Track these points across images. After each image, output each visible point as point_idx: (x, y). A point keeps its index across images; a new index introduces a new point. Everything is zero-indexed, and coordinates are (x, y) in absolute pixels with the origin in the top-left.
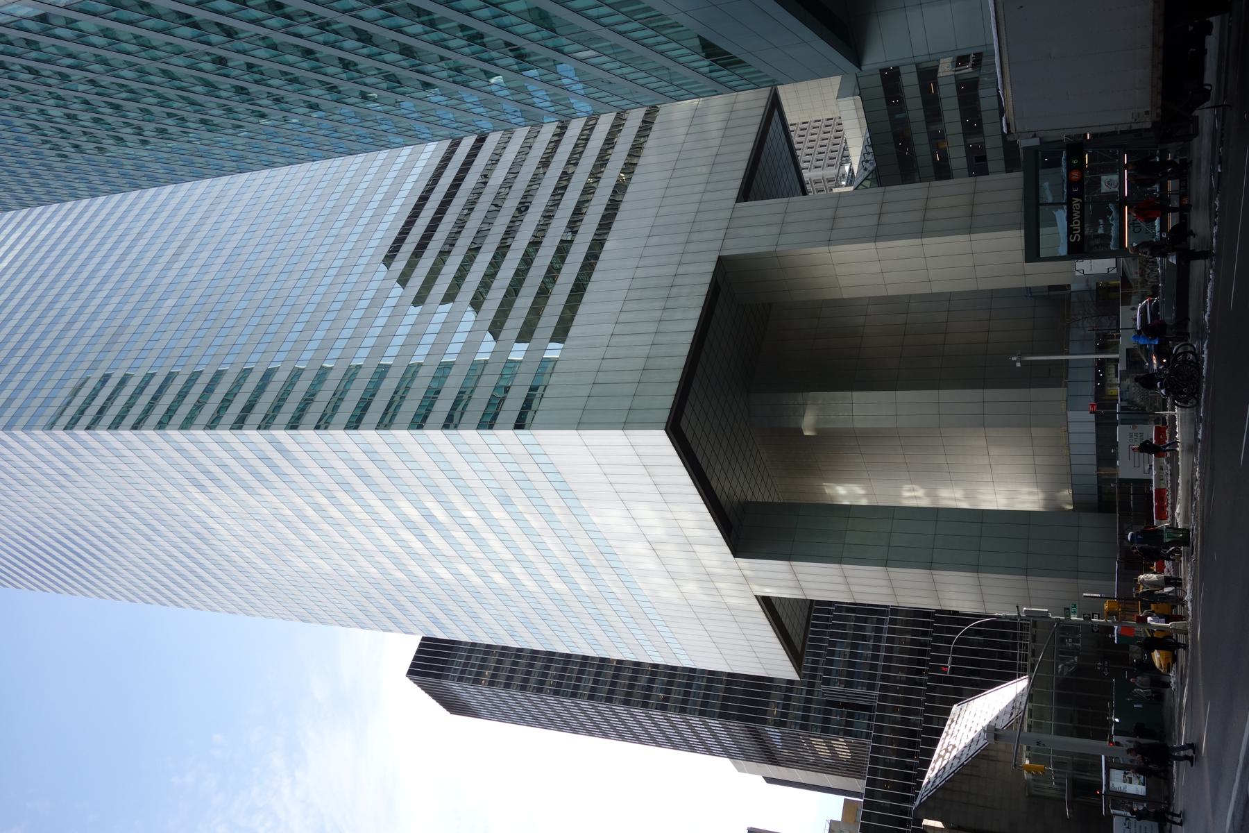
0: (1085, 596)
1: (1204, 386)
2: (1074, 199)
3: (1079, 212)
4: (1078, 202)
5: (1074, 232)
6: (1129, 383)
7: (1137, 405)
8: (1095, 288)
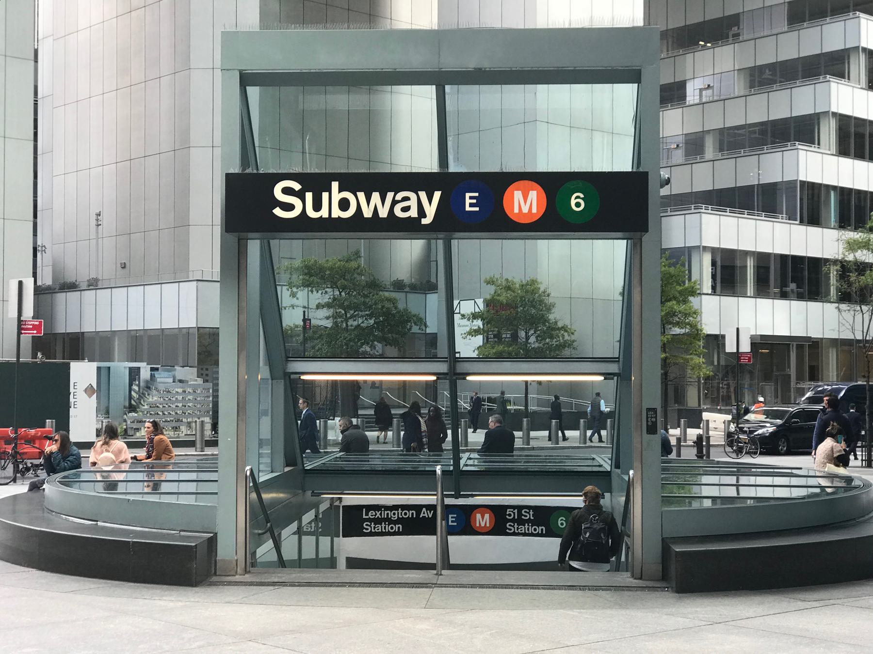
1: (834, 387)
2: (437, 195)
3: (383, 213)
4: (422, 213)
5: (309, 196)
7: (142, 396)
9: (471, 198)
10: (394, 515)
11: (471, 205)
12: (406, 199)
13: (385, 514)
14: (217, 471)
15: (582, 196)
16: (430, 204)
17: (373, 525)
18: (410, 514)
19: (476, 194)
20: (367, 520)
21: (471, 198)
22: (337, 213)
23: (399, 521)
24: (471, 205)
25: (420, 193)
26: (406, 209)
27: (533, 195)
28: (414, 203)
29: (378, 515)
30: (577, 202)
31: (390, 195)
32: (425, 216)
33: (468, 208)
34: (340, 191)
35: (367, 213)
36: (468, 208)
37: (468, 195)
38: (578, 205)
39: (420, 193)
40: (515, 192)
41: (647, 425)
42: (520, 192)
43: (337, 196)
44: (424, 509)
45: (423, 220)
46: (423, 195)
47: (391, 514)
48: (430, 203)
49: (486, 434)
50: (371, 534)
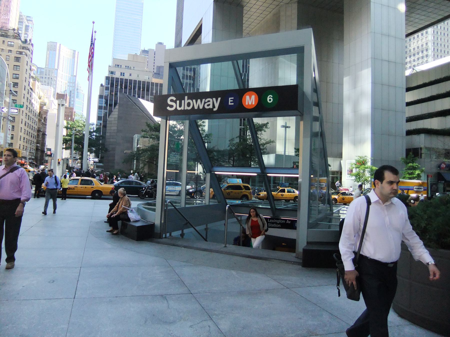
0: (298, 174)
2: (219, 99)
3: (201, 107)
4: (214, 106)
5: (178, 102)
6: (23, 161)
8: (38, 111)
9: (231, 100)
11: (231, 102)
12: (209, 101)
14: (349, 205)
15: (272, 96)
16: (217, 103)
18: (283, 221)
19: (233, 98)
21: (231, 100)
22: (186, 108)
23: (279, 224)
24: (231, 102)
25: (213, 99)
26: (208, 105)
27: (253, 97)
28: (211, 103)
30: (270, 99)
31: (204, 100)
33: (230, 104)
34: (188, 100)
35: (196, 107)
36: (230, 104)
37: (230, 98)
38: (270, 100)
39: (213, 99)
40: (247, 96)
42: (248, 96)
44: (288, 221)
45: (214, 109)
46: (214, 99)
47: (277, 221)
49: (419, 200)
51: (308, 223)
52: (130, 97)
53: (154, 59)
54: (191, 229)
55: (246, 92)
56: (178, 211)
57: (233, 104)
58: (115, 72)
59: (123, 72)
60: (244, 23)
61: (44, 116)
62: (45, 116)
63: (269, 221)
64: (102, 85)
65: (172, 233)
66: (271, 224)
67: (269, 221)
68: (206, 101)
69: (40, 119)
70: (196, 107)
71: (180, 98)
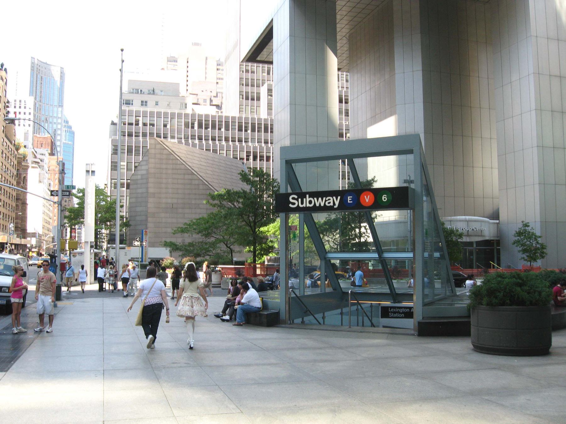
2: (339, 198)
3: (322, 205)
5: (300, 200)
9: (350, 198)
10: (401, 311)
11: (350, 201)
12: (329, 199)
13: (397, 310)
15: (386, 196)
17: (393, 314)
19: (351, 197)
20: (390, 312)
21: (350, 198)
22: (308, 205)
23: (403, 313)
24: (350, 201)
26: (329, 203)
28: (331, 201)
29: (395, 310)
30: (384, 198)
31: (324, 198)
32: (335, 205)
34: (309, 198)
35: (317, 205)
36: (349, 202)
37: (349, 197)
38: (385, 199)
41: (58, 229)
43: (308, 199)
46: (334, 198)
47: (400, 310)
48: (337, 200)
50: (392, 317)
51: (423, 302)
52: (166, 143)
53: (189, 69)
54: (311, 317)
55: (362, 192)
56: (299, 299)
57: (352, 202)
58: (132, 101)
59: (144, 100)
60: (337, 22)
61: (23, 176)
62: (25, 175)
63: (390, 310)
64: (113, 124)
65: (295, 320)
66: (393, 314)
67: (390, 310)
68: (327, 199)
69: (19, 181)
70: (317, 205)
71: (302, 195)
